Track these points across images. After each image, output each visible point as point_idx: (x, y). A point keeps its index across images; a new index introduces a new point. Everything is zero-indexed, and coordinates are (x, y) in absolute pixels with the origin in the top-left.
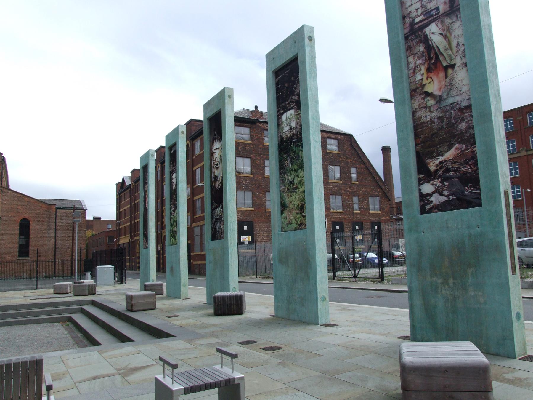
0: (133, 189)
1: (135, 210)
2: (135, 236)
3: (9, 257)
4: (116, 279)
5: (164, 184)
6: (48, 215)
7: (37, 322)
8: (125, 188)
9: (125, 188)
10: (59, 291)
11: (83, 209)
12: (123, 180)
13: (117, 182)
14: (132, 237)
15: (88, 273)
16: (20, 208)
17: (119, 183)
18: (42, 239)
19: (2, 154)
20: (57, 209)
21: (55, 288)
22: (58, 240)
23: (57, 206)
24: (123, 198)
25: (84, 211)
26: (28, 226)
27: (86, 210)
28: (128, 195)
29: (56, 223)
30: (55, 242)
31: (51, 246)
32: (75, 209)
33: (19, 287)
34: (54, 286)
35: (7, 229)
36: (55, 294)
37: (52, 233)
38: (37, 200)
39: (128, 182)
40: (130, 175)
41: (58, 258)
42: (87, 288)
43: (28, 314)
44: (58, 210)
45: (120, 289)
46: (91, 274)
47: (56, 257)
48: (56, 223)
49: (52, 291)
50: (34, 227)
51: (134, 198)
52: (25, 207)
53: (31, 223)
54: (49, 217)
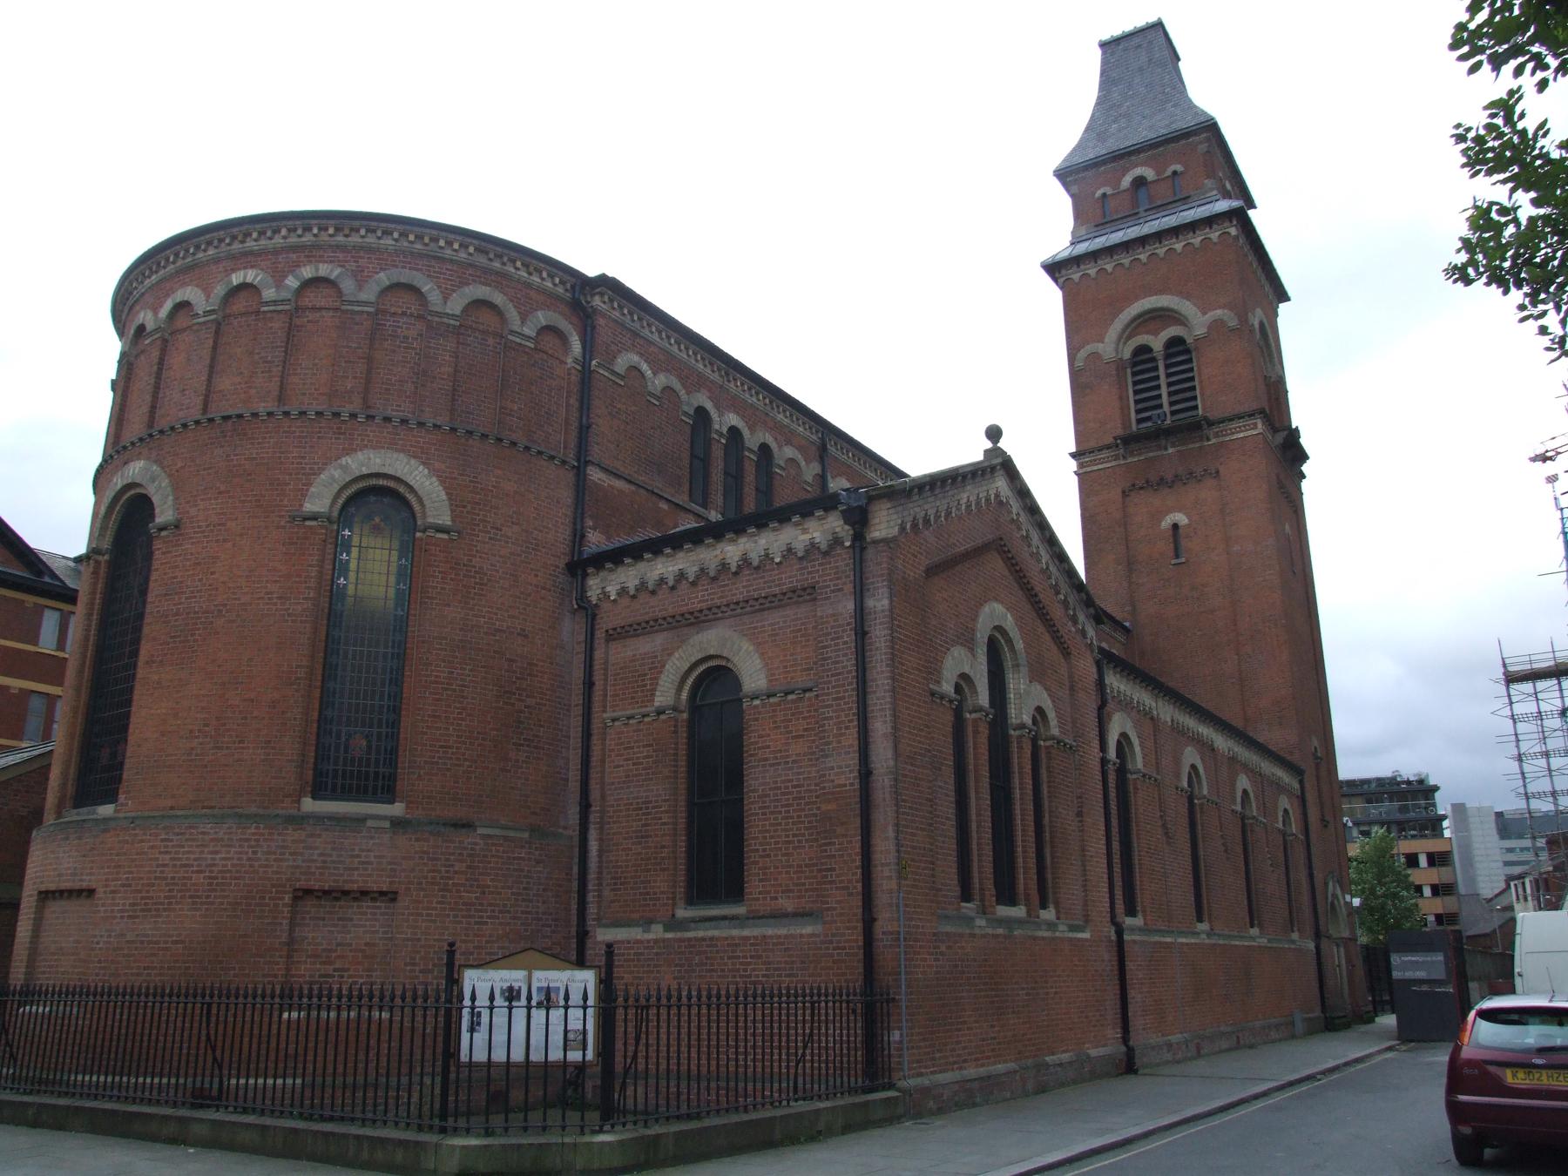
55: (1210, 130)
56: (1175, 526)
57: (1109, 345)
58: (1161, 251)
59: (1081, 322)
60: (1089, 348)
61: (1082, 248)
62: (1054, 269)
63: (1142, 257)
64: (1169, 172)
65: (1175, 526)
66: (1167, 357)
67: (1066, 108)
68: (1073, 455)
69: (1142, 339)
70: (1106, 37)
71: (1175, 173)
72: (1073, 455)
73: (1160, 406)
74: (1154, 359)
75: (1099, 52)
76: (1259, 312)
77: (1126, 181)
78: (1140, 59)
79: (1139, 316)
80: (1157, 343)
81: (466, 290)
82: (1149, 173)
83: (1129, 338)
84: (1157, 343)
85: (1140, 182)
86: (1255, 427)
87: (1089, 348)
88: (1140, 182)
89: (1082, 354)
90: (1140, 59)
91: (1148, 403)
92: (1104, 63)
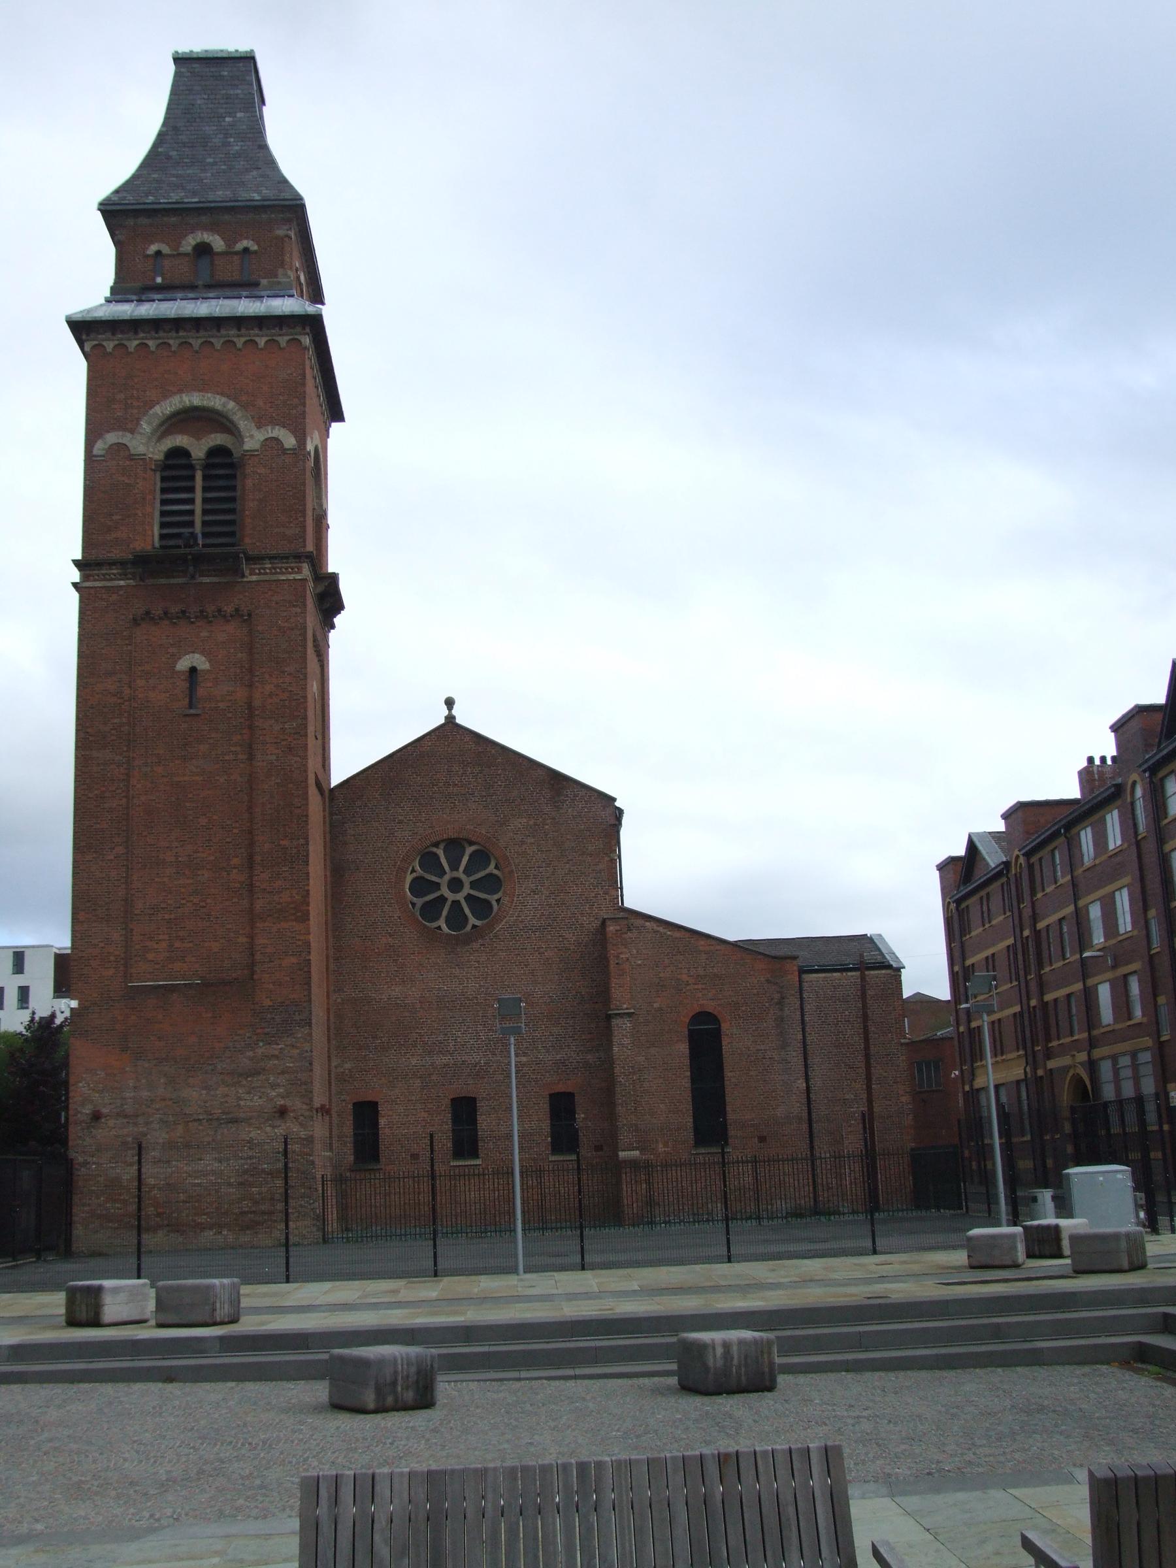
0: (1018, 880)
1: (1039, 954)
2: (1049, 1055)
3: (666, 1145)
4: (1142, 1215)
5: (1167, 848)
6: (777, 996)
7: (1035, 1359)
8: (979, 877)
9: (979, 877)
10: (985, 1260)
11: (890, 967)
12: (972, 846)
13: (941, 857)
14: (1032, 1060)
15: (1046, 1196)
16: (685, 977)
17: (952, 860)
18: (767, 1083)
19: (614, 800)
20: (802, 971)
21: (972, 1246)
22: (817, 1083)
23: (800, 962)
24: (975, 916)
25: (893, 972)
26: (716, 1035)
27: (898, 970)
28: (996, 902)
29: (803, 1022)
30: (808, 1087)
31: (796, 1106)
32: (863, 967)
33: (612, 1258)
34: (970, 1239)
35: (653, 1051)
36: (972, 1267)
37: (795, 1057)
38: (736, 945)
39: (993, 857)
40: (1000, 826)
41: (823, 1149)
42: (1123, 1245)
43: (997, 1333)
44: (806, 977)
45: (571, 1297)
46: (1054, 1198)
47: (816, 1143)
48: (803, 1022)
49: (960, 1257)
50: (736, 1041)
51: (1027, 913)
52: (701, 972)
53: (724, 1027)
54: (781, 1003)
55: (293, 211)
56: (193, 670)
57: (146, 443)
58: (283, 341)
59: (105, 409)
60: (112, 438)
61: (126, 310)
62: (83, 329)
63: (150, 343)
64: (240, 246)
65: (193, 670)
66: (207, 467)
67: (124, 130)
68: (76, 563)
69: (180, 440)
70: (184, 48)
71: (246, 250)
72: (76, 563)
73: (191, 524)
74: (191, 467)
75: (171, 68)
76: (316, 435)
77: (189, 243)
78: (216, 94)
79: (175, 415)
80: (198, 449)
81: (157, 409)
82: (218, 243)
83: (160, 439)
84: (198, 449)
85: (203, 250)
86: (300, 571)
87: (112, 438)
88: (203, 250)
89: (99, 447)
90: (216, 94)
91: (174, 523)
92: (177, 75)
